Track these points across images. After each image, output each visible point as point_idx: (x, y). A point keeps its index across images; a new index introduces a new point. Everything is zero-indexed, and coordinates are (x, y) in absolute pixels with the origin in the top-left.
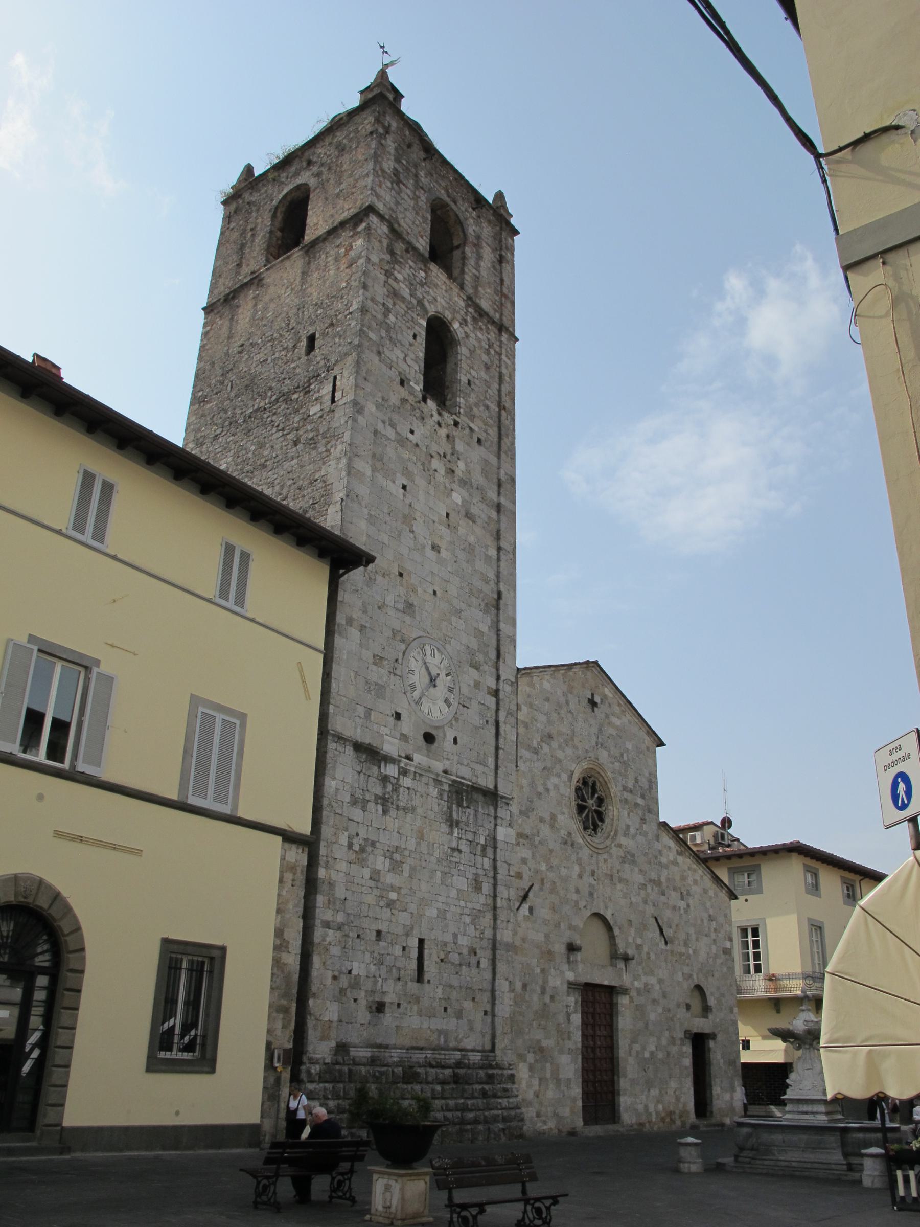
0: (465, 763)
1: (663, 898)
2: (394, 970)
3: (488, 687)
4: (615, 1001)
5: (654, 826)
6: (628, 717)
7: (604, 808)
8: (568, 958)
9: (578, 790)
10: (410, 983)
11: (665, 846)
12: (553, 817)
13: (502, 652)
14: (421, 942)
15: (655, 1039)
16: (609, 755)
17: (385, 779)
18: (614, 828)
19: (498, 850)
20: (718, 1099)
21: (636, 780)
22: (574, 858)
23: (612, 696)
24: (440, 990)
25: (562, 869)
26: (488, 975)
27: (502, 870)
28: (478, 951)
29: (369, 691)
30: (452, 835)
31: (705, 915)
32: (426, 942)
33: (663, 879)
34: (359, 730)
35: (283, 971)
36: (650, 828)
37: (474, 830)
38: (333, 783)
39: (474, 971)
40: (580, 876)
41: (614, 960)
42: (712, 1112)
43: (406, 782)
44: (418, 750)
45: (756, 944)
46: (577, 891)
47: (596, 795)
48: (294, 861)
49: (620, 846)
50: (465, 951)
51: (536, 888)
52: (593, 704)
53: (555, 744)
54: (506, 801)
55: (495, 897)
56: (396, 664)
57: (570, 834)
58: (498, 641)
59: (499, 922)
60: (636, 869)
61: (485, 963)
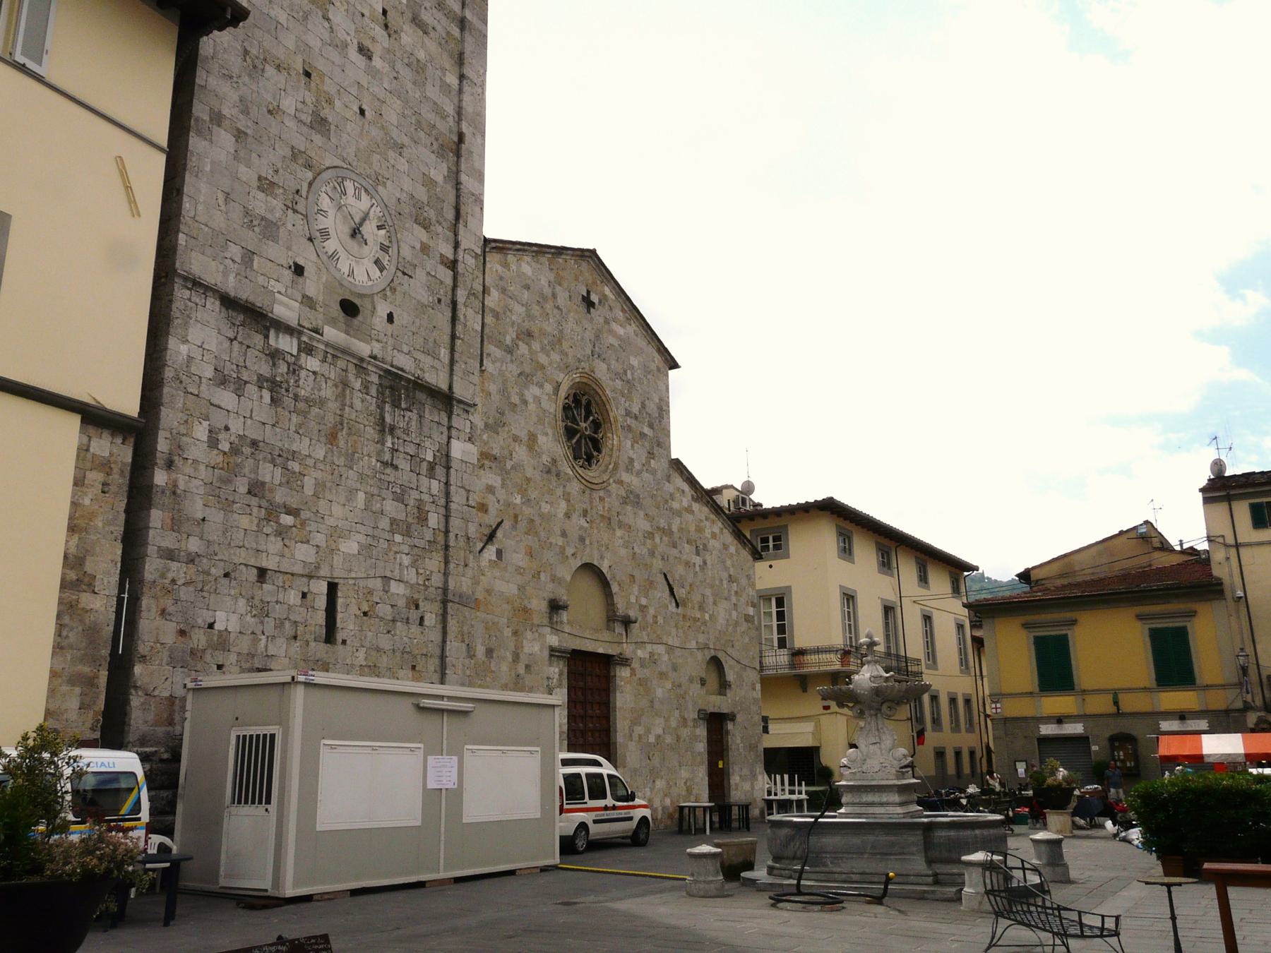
0: (405, 349)
1: (675, 552)
2: (287, 624)
3: (441, 254)
4: (612, 674)
5: (665, 464)
6: (632, 329)
8: (551, 618)
9: (566, 408)
10: (313, 644)
11: (678, 489)
12: (532, 438)
13: (401, 366)
14: (333, 588)
15: (662, 720)
16: (608, 369)
17: (274, 355)
18: (613, 460)
19: (452, 471)
20: (737, 789)
21: (643, 406)
22: (559, 491)
23: (613, 298)
24: (361, 654)
25: (543, 504)
26: (436, 636)
27: (458, 498)
28: (421, 604)
29: (251, 226)
30: (383, 444)
31: (725, 575)
32: (339, 587)
33: (675, 528)
34: (231, 278)
35: (81, 621)
36: (659, 465)
37: (418, 442)
38: (184, 349)
39: (415, 629)
40: (568, 516)
41: (611, 624)
43: (312, 363)
44: (333, 322)
45: (781, 616)
46: (564, 534)
47: (591, 418)
48: (107, 454)
49: (620, 482)
50: (401, 603)
51: (507, 525)
52: (589, 304)
53: (536, 346)
54: (466, 408)
55: (447, 532)
56: (297, 197)
57: (554, 461)
58: (458, 197)
59: (452, 566)
60: (642, 513)
61: (430, 619)
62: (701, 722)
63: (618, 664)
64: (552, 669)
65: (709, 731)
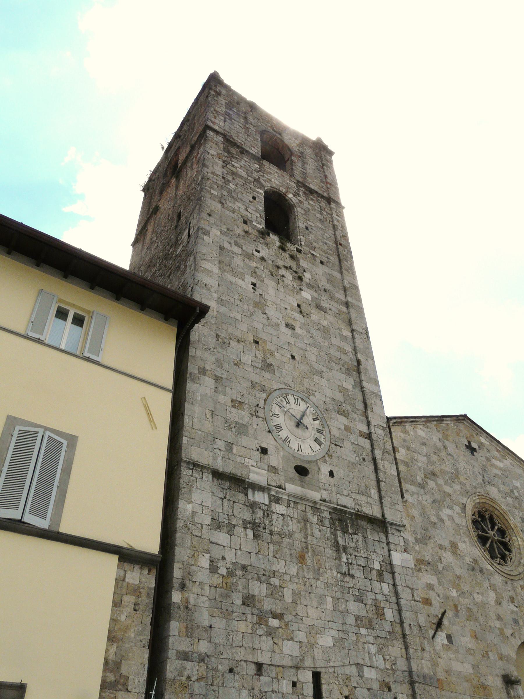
23: (488, 443)
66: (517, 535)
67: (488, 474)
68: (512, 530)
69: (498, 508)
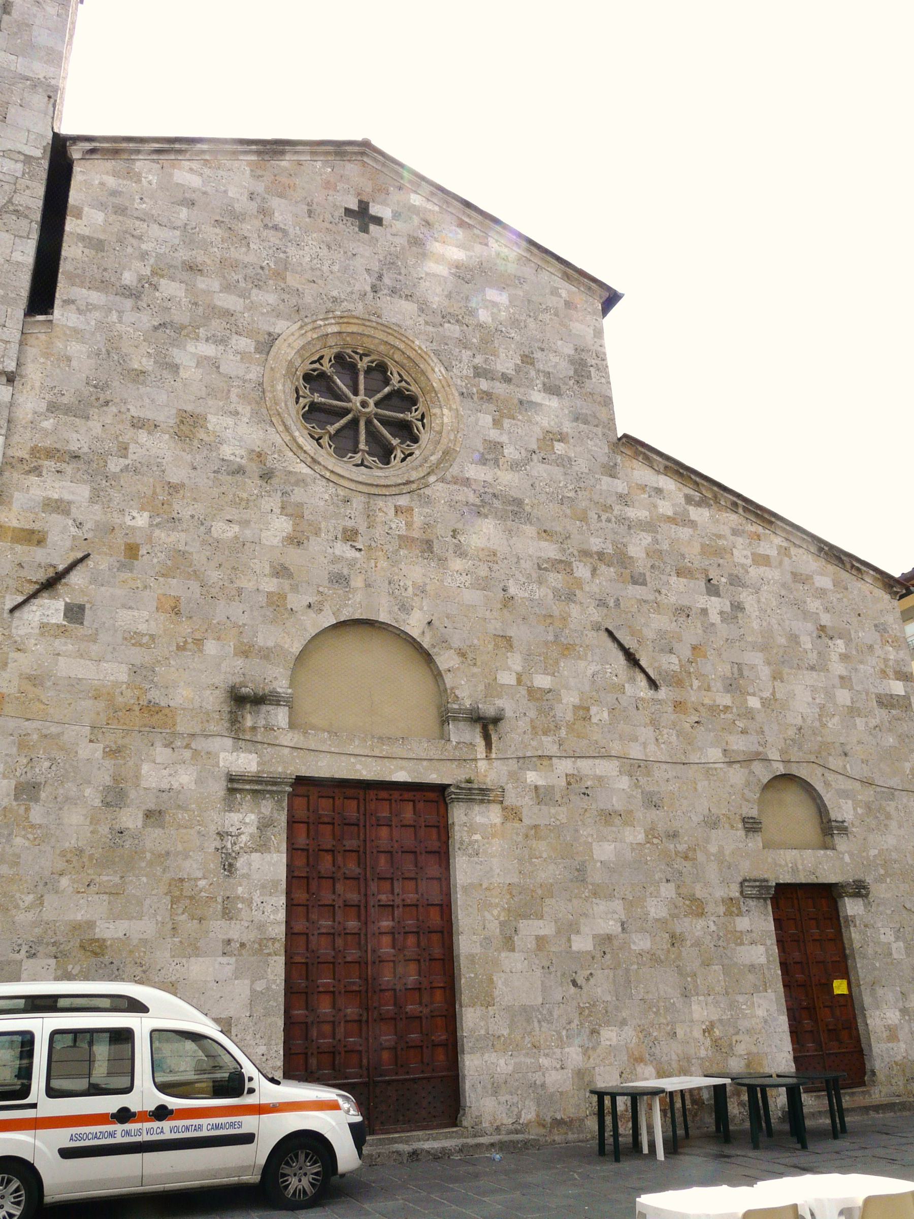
7: (418, 414)
23: (437, 209)
42: (873, 1073)
51: (101, 562)
62: (752, 903)
63: (459, 800)
64: (235, 817)
65: (778, 922)
66: (443, 403)
67: (400, 274)
68: (433, 395)
69: (402, 346)
